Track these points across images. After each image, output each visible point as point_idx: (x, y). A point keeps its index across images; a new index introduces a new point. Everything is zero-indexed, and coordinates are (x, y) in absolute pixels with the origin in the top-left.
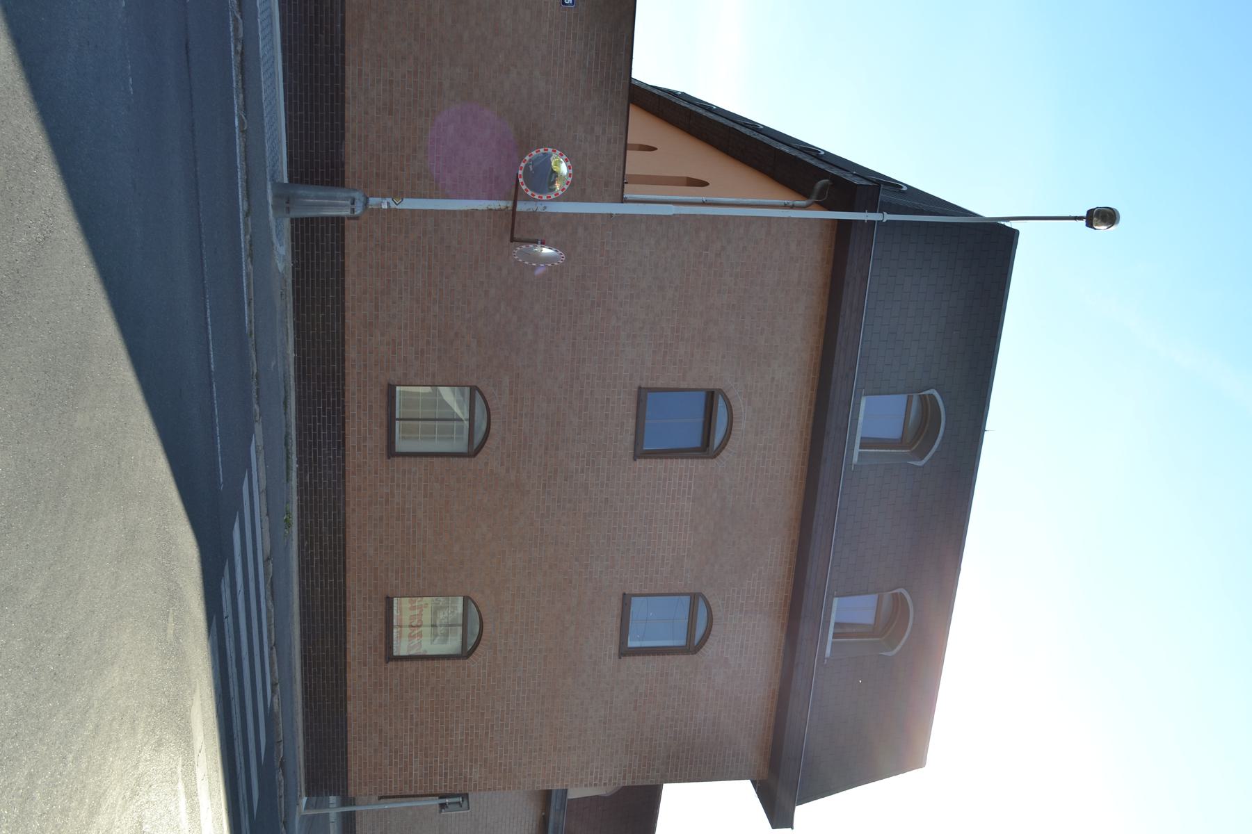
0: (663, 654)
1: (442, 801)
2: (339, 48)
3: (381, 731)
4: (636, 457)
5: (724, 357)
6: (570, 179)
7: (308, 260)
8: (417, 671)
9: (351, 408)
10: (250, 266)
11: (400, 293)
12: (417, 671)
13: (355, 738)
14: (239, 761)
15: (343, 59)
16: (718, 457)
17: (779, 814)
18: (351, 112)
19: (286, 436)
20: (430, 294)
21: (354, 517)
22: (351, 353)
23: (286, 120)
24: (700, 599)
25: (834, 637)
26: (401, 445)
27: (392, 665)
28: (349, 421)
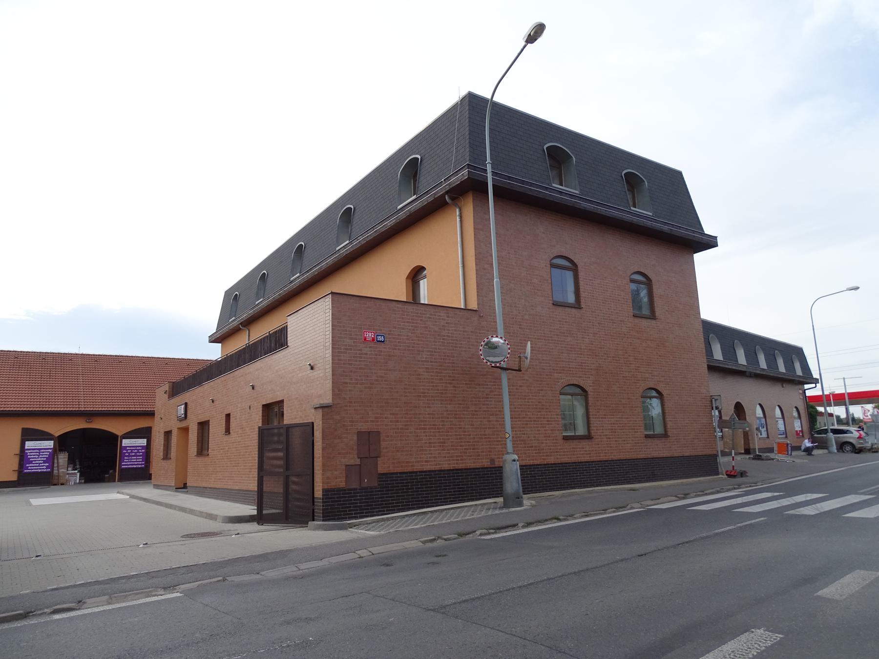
0: (579, 286)
1: (714, 408)
2: (412, 475)
3: (693, 439)
4: (580, 308)
5: (536, 259)
6: (507, 342)
7: (346, 501)
8: (670, 421)
9: (574, 459)
10: (691, 495)
11: (524, 434)
12: (670, 421)
13: (659, 453)
14: (292, 573)
15: (420, 472)
16: (577, 264)
17: (709, 243)
18: (446, 466)
19: (628, 490)
20: (524, 418)
21: (616, 456)
22: (552, 460)
23: (490, 498)
24: (552, 261)
25: (562, 186)
26: (581, 431)
27: (669, 433)
28: (580, 460)
